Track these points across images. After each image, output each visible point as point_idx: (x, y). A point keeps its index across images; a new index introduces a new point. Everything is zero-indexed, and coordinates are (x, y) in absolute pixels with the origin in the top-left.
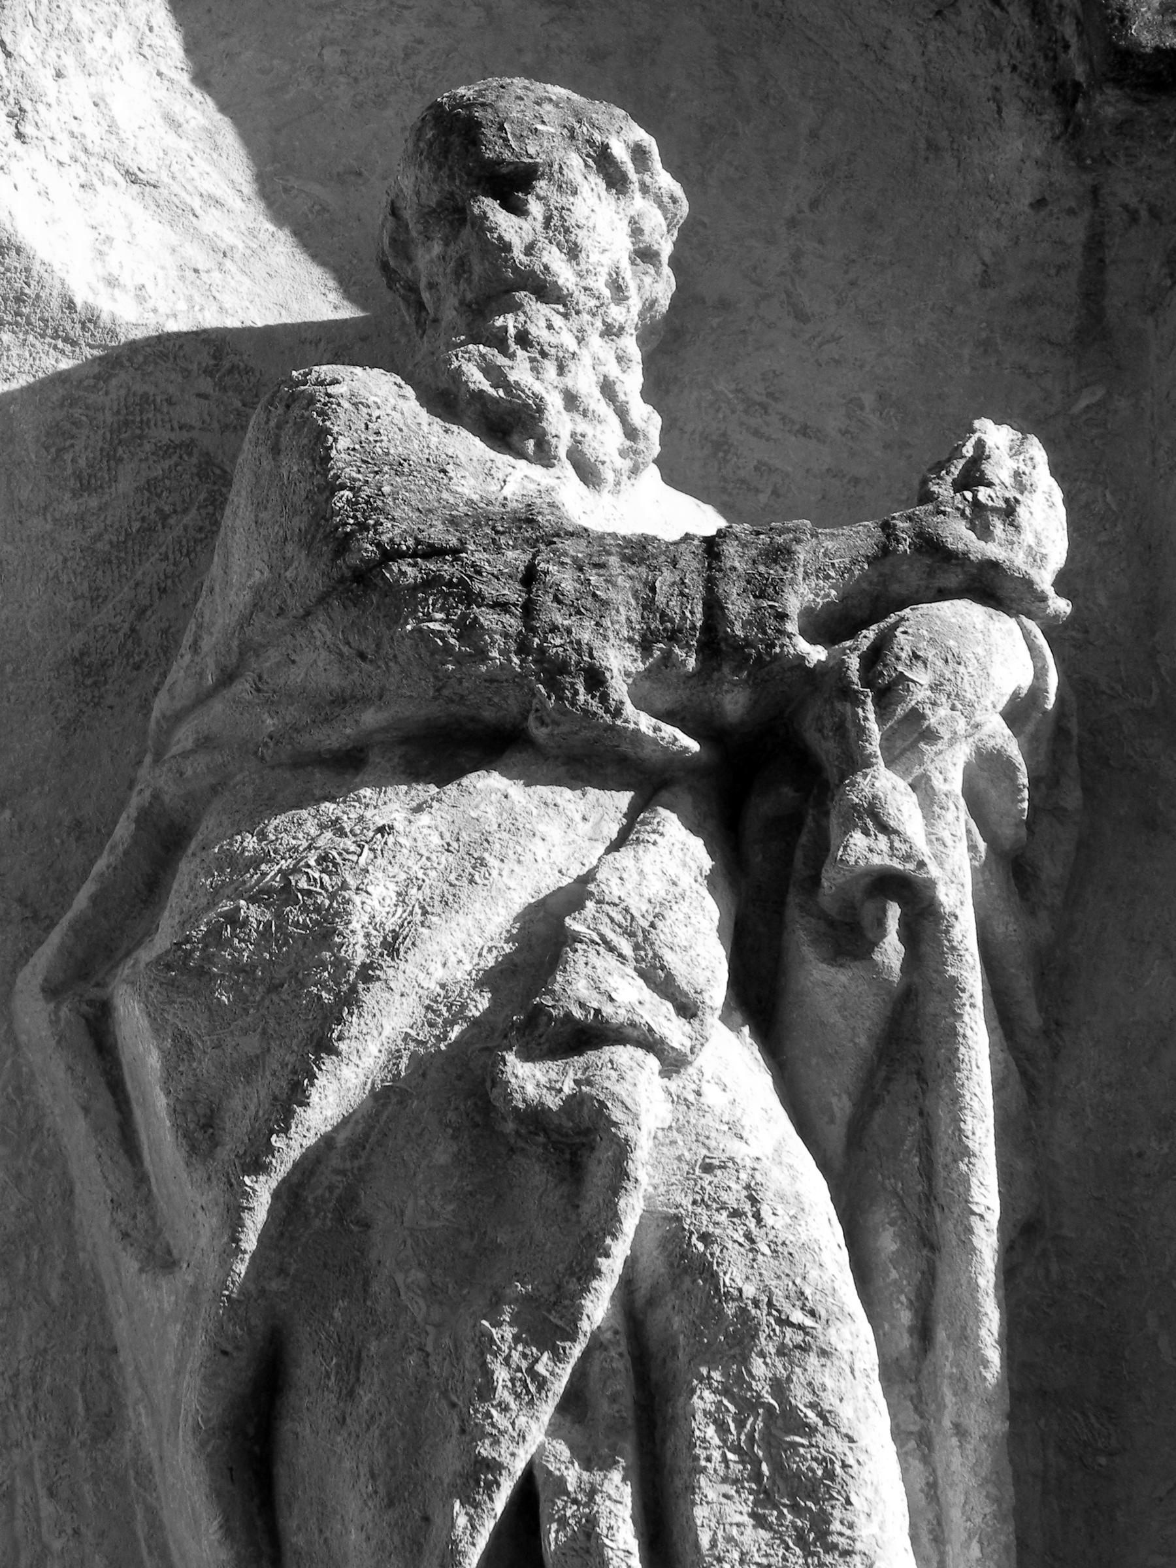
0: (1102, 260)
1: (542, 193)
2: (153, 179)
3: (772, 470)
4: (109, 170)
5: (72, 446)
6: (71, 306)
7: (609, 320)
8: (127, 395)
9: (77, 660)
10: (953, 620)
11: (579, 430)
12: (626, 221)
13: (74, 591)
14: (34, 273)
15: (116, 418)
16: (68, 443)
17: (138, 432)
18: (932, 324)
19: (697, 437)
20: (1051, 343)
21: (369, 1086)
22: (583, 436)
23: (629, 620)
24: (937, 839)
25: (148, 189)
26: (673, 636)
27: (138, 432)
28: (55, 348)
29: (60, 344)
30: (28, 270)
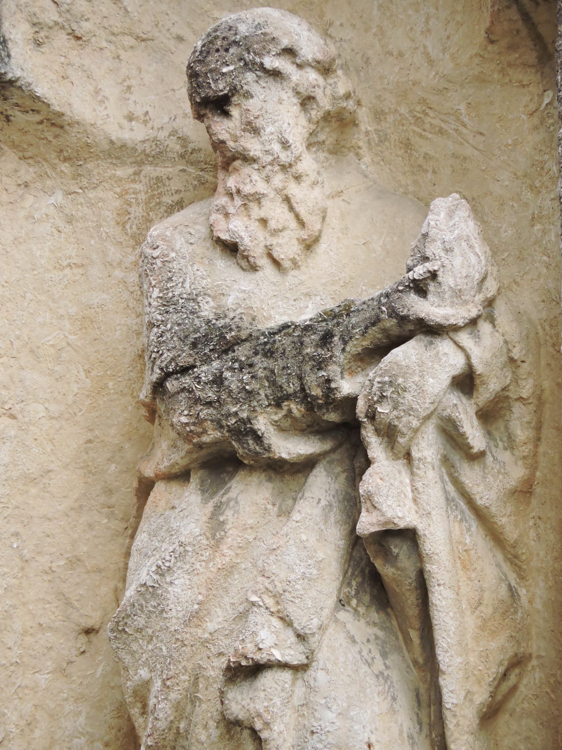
1: (236, 103)
2: (149, 36)
3: (431, 158)
4: (129, 41)
5: (129, 218)
6: (112, 142)
7: (282, 163)
8: (150, 180)
9: (141, 356)
10: (403, 363)
11: (268, 244)
12: (291, 91)
16: (127, 218)
19: (397, 143)
20: (529, 66)
22: (271, 245)
23: (266, 396)
24: (416, 489)
26: (287, 397)
28: (112, 163)
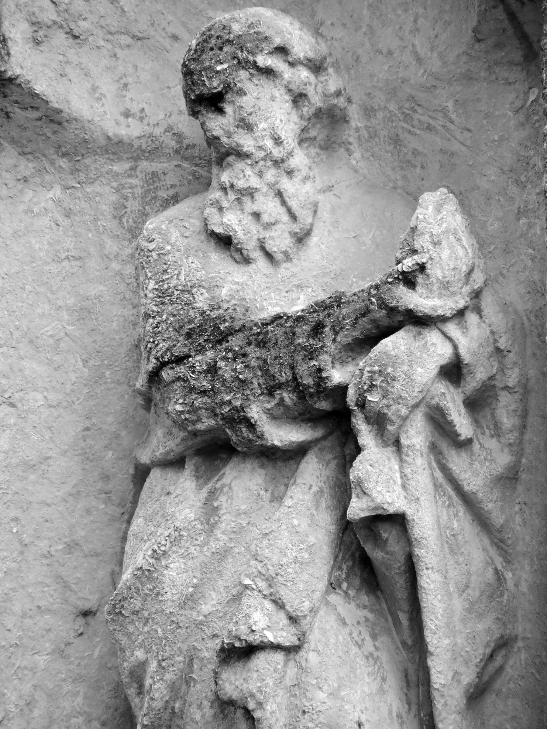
0: (519, 23)
1: (229, 100)
2: (146, 34)
4: (125, 40)
5: (126, 212)
6: (109, 138)
7: (274, 159)
8: (146, 175)
10: (392, 353)
11: (261, 237)
12: (283, 88)
13: (133, 303)
14: (86, 128)
15: (143, 190)
17: (153, 195)
18: (465, 63)
21: (518, 326)
23: (259, 385)
25: (145, 41)
26: (280, 386)
27: (153, 195)
28: (109, 158)
29: (111, 157)
30: (83, 127)
